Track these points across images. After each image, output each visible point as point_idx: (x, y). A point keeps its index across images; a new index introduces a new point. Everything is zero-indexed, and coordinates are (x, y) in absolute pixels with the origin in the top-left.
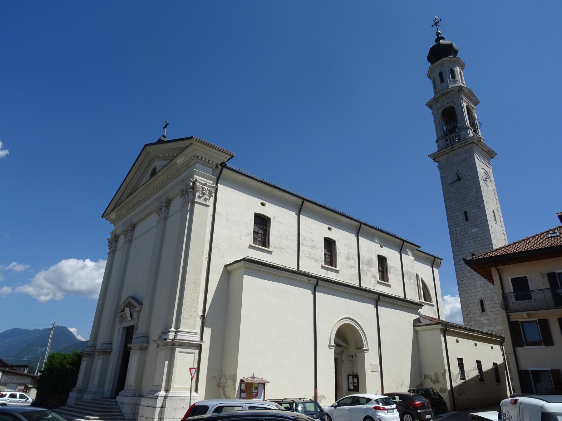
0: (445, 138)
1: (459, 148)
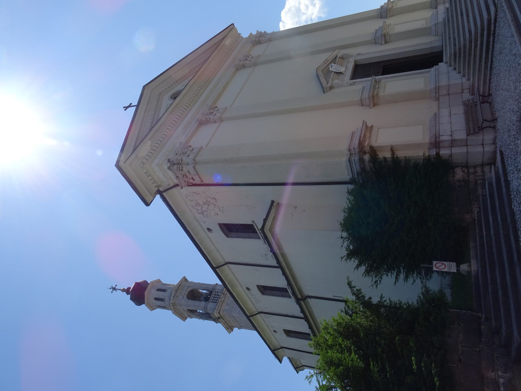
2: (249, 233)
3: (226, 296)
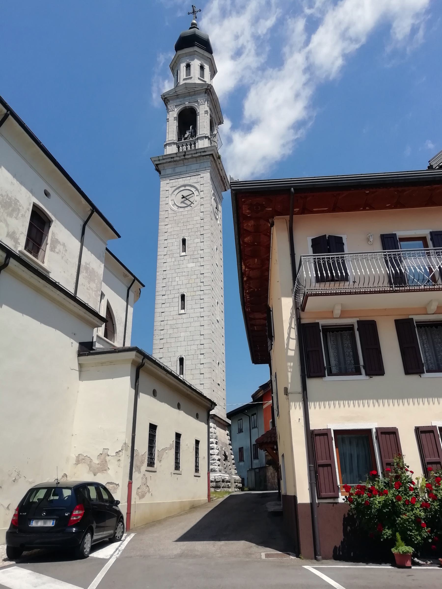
1: (192, 157)
3: (185, 161)
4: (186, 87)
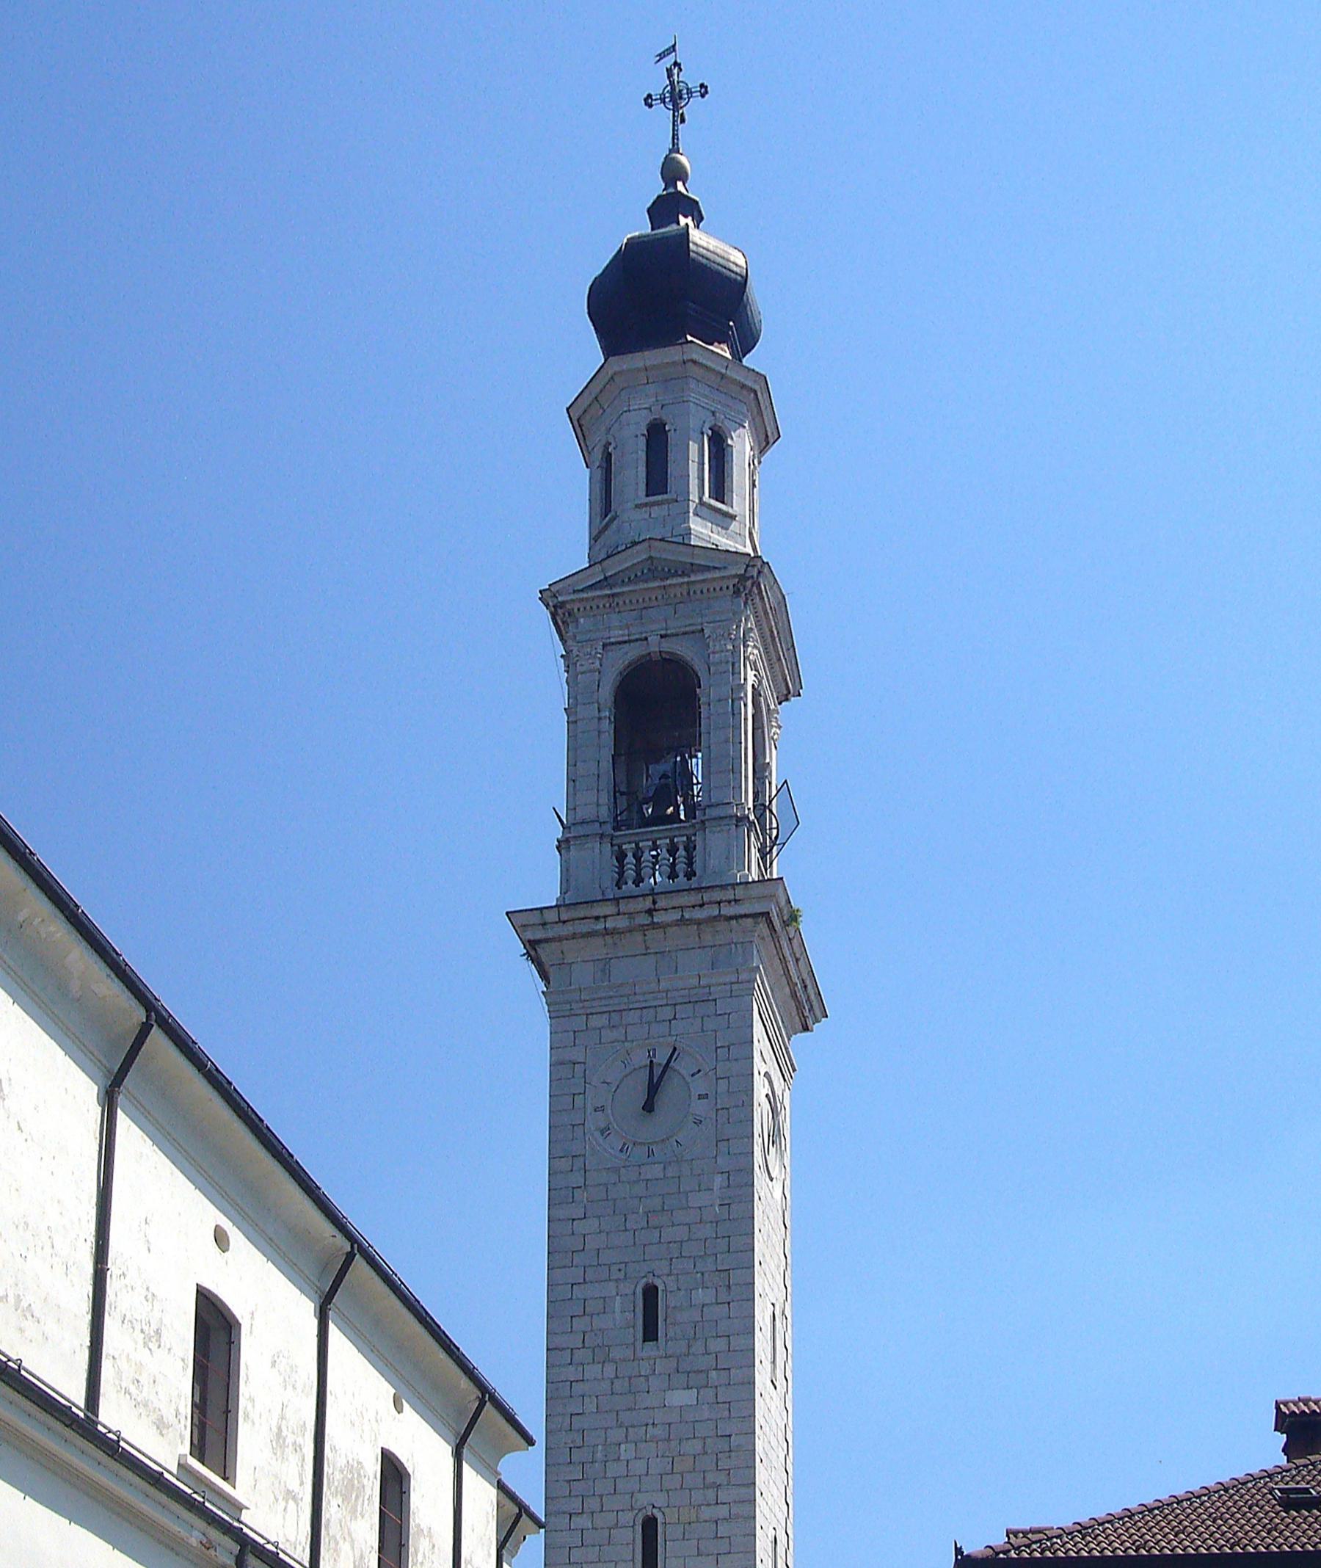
0: (612, 837)
1: (682, 922)
2: (73, 1391)
3: (651, 934)
4: (651, 558)
